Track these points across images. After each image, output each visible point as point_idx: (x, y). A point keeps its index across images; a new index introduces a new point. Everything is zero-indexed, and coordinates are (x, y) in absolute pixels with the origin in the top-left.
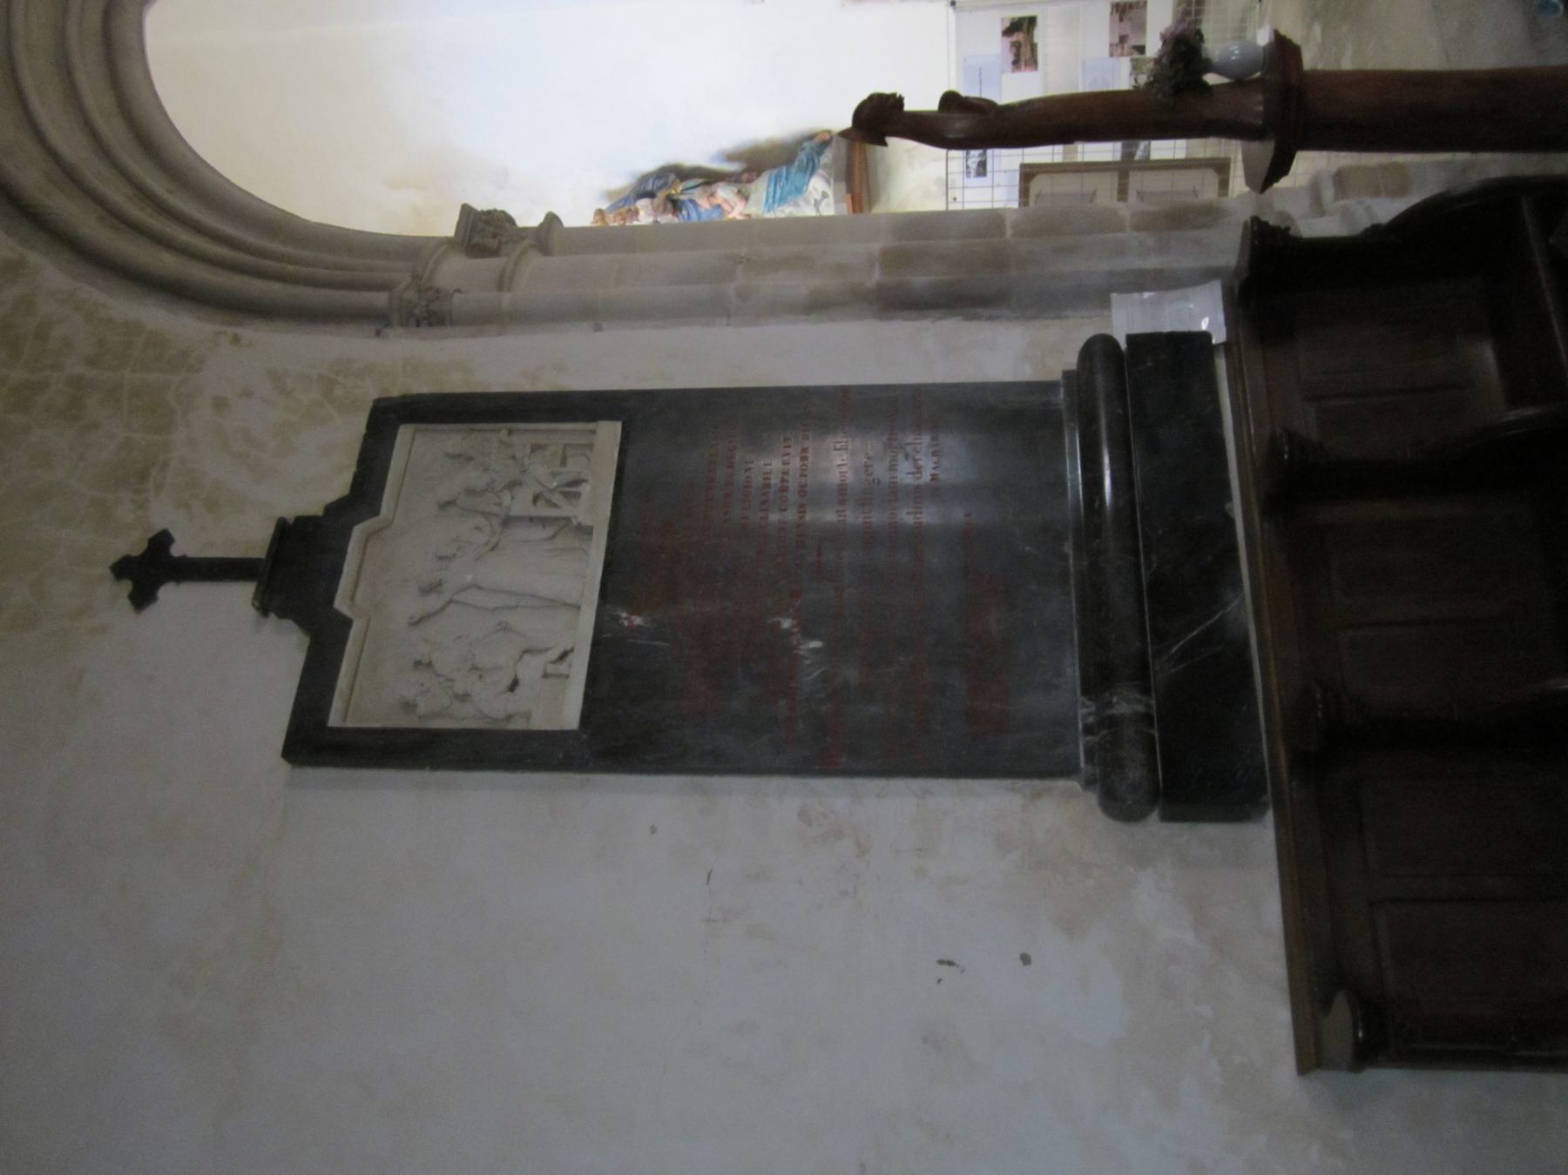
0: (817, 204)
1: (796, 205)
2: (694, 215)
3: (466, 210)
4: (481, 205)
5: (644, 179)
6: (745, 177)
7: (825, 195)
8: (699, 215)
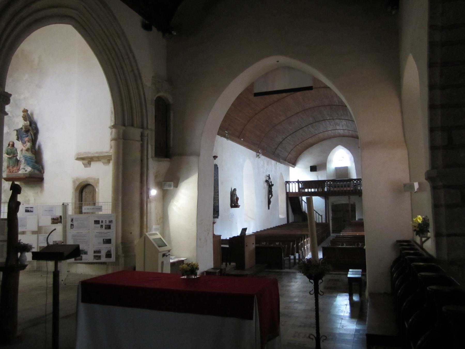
0: (24, 169)
1: (24, 163)
2: (24, 136)
3: (10, 95)
4: (11, 98)
5: (36, 124)
6: (33, 150)
7: (26, 171)
8: (24, 137)
